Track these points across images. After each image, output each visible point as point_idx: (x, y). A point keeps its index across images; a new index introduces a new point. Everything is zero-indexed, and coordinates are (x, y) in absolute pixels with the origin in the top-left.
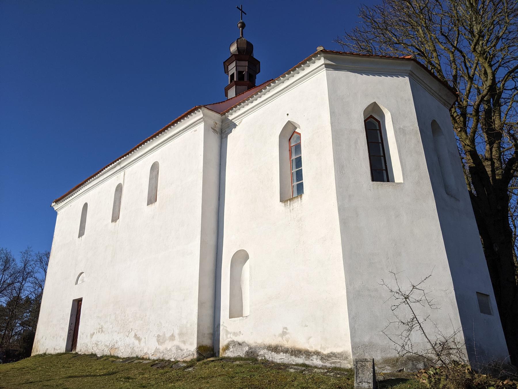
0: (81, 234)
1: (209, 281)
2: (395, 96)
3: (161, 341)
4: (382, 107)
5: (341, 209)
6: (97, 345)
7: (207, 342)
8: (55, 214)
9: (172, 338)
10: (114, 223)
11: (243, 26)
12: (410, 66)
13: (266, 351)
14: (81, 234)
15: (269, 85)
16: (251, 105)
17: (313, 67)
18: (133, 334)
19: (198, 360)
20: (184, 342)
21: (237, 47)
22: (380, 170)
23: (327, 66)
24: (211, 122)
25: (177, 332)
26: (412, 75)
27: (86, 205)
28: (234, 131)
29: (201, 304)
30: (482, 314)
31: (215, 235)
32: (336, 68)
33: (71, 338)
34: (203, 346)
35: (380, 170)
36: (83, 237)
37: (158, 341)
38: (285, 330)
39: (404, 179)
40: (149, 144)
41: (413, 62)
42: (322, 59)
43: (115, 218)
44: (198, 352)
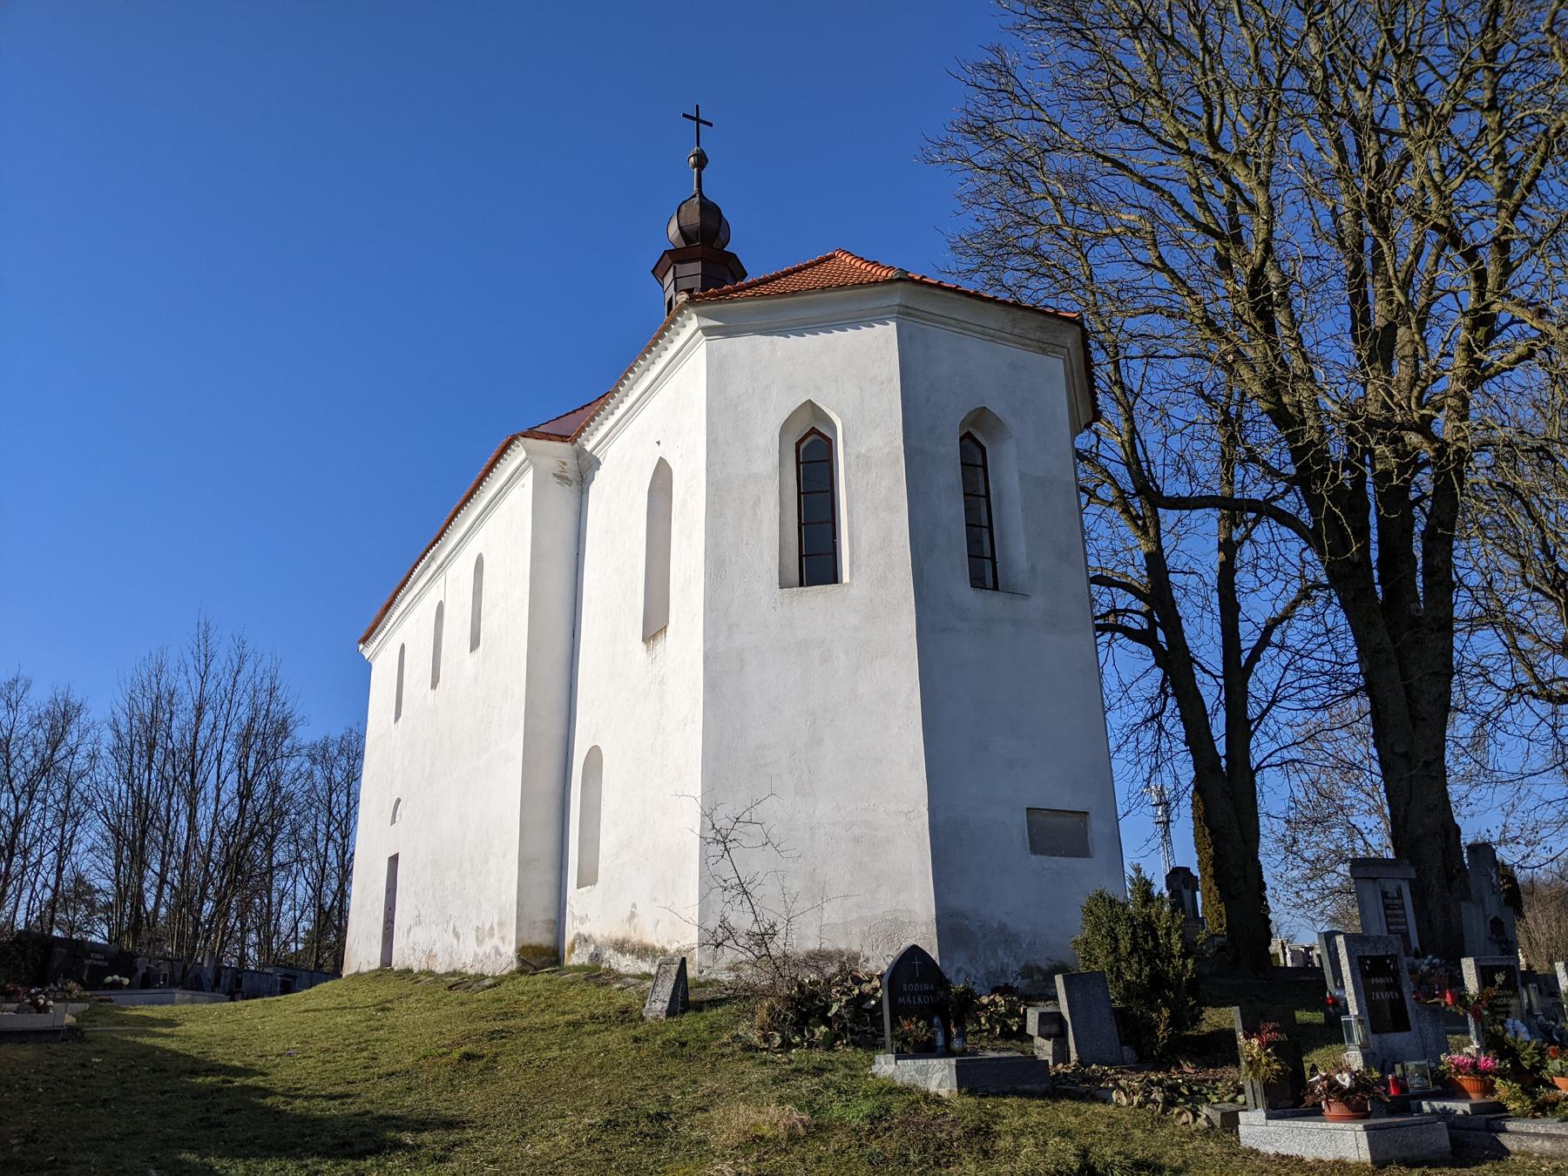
1: (545, 813)
4: (827, 411)
5: (708, 659)
7: (541, 938)
8: (368, 667)
11: (701, 161)
15: (627, 378)
16: (613, 420)
19: (521, 972)
21: (680, 228)
22: (816, 560)
23: (707, 331)
24: (551, 464)
28: (600, 475)
29: (525, 863)
30: (1035, 859)
31: (564, 715)
32: (727, 332)
34: (530, 946)
35: (816, 560)
40: (467, 515)
41: (900, 285)
42: (695, 317)
44: (519, 958)
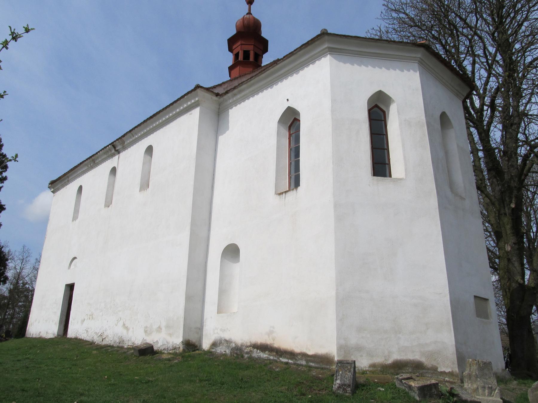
0: (75, 218)
2: (406, 87)
3: (148, 332)
6: (87, 331)
9: (159, 329)
10: (107, 208)
12: (420, 54)
13: (251, 348)
14: (75, 218)
17: (413, 55)
18: (121, 323)
20: (171, 335)
22: (381, 166)
25: (163, 324)
26: (422, 63)
27: (81, 187)
33: (64, 323)
35: (381, 166)
36: (77, 221)
37: (146, 332)
38: (272, 329)
39: (406, 175)
41: (422, 49)
43: (108, 204)
